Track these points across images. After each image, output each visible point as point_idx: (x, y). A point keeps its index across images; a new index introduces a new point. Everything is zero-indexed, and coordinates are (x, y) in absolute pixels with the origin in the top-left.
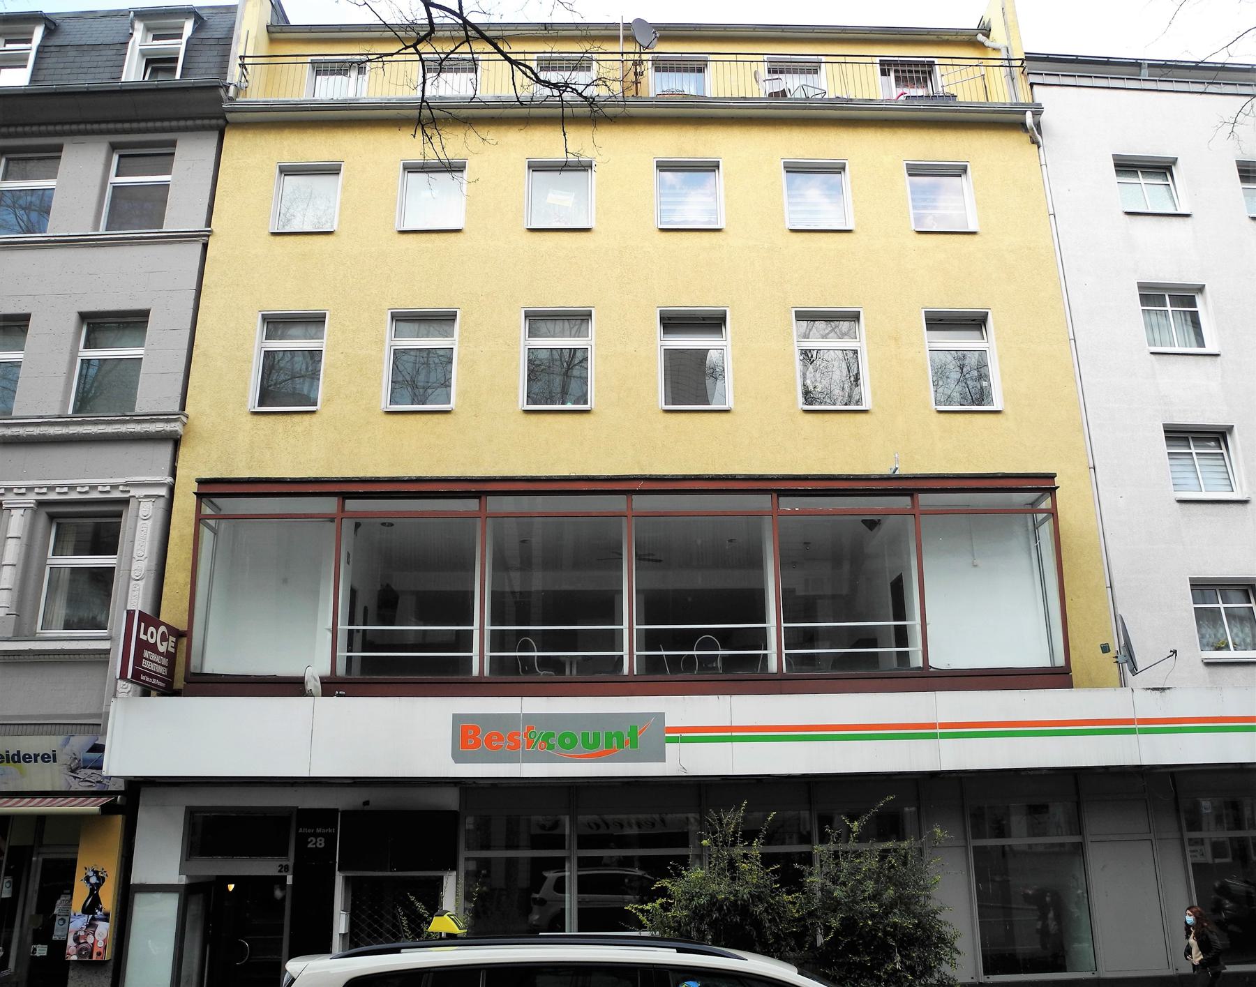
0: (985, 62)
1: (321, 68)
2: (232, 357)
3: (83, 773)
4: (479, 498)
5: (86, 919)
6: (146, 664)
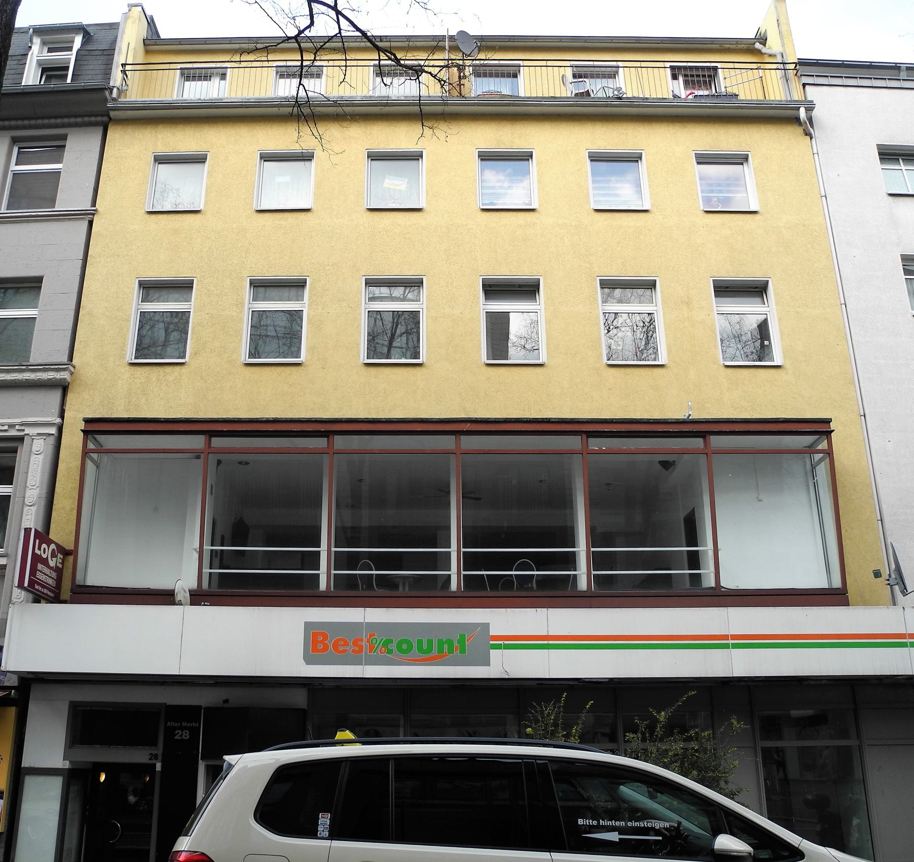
0: (762, 66)
1: (189, 75)
2: (113, 314)
4: (327, 436)
6: (39, 575)
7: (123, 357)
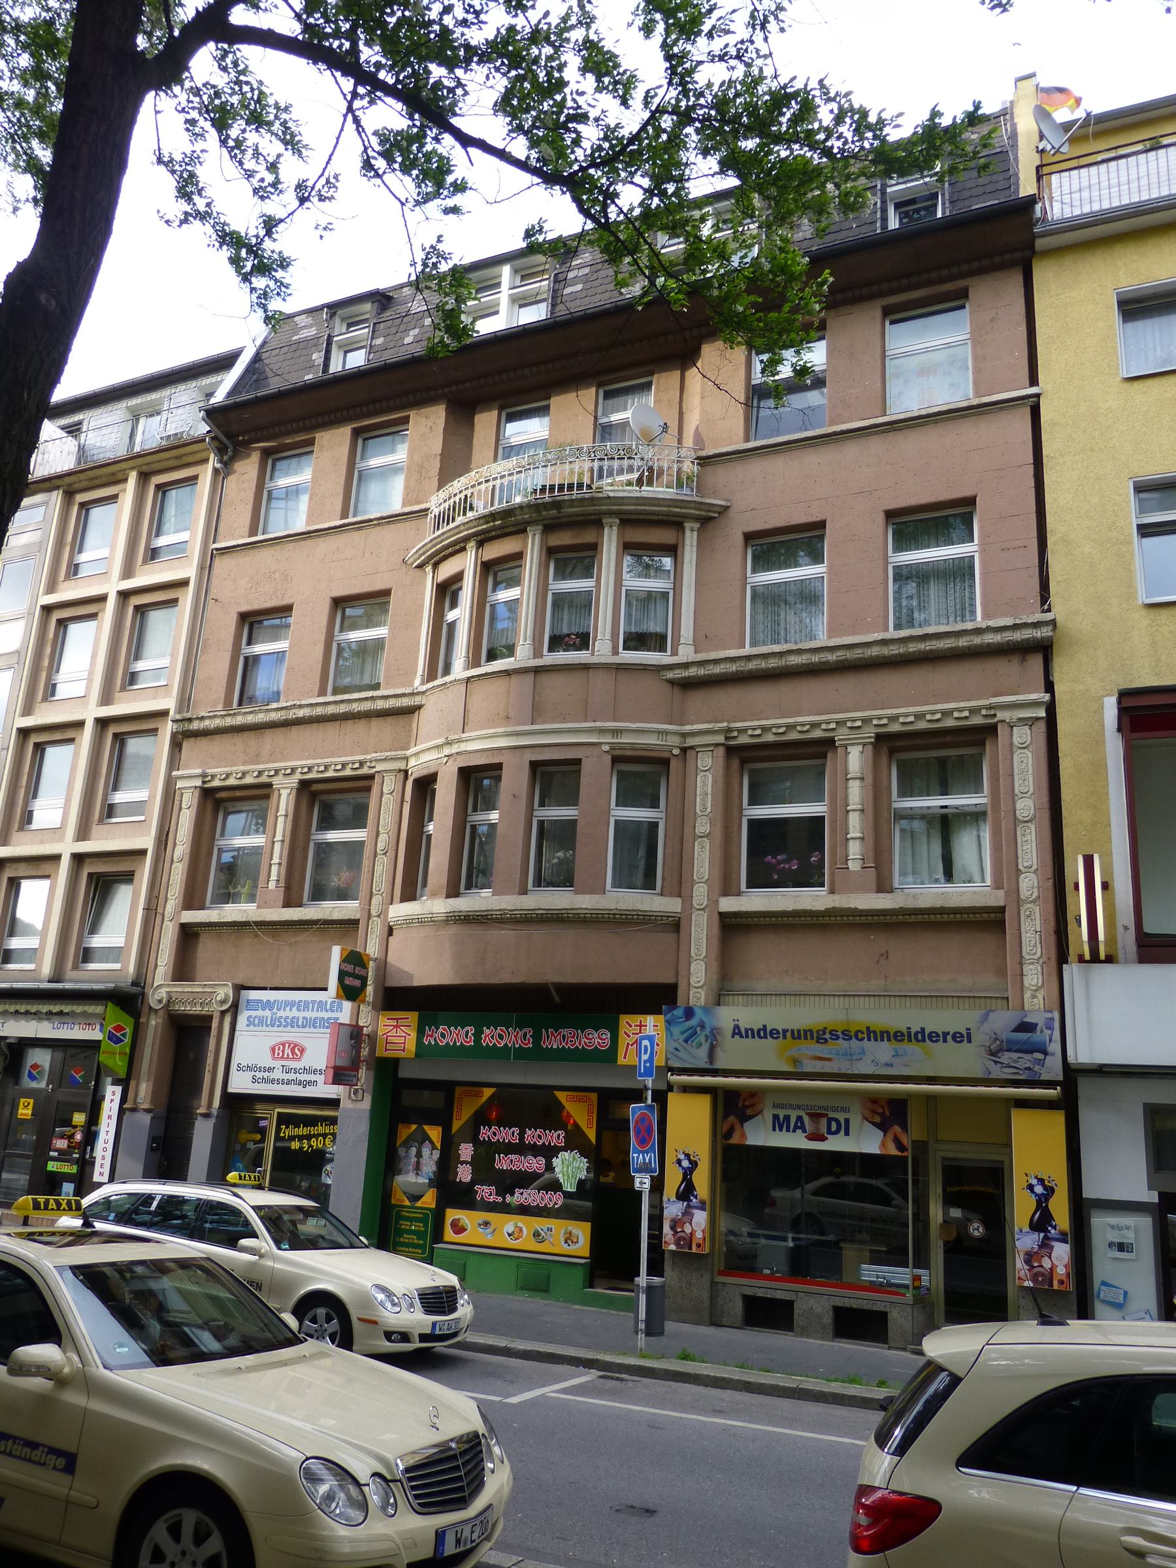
3: (1006, 1057)
7: (1132, 596)
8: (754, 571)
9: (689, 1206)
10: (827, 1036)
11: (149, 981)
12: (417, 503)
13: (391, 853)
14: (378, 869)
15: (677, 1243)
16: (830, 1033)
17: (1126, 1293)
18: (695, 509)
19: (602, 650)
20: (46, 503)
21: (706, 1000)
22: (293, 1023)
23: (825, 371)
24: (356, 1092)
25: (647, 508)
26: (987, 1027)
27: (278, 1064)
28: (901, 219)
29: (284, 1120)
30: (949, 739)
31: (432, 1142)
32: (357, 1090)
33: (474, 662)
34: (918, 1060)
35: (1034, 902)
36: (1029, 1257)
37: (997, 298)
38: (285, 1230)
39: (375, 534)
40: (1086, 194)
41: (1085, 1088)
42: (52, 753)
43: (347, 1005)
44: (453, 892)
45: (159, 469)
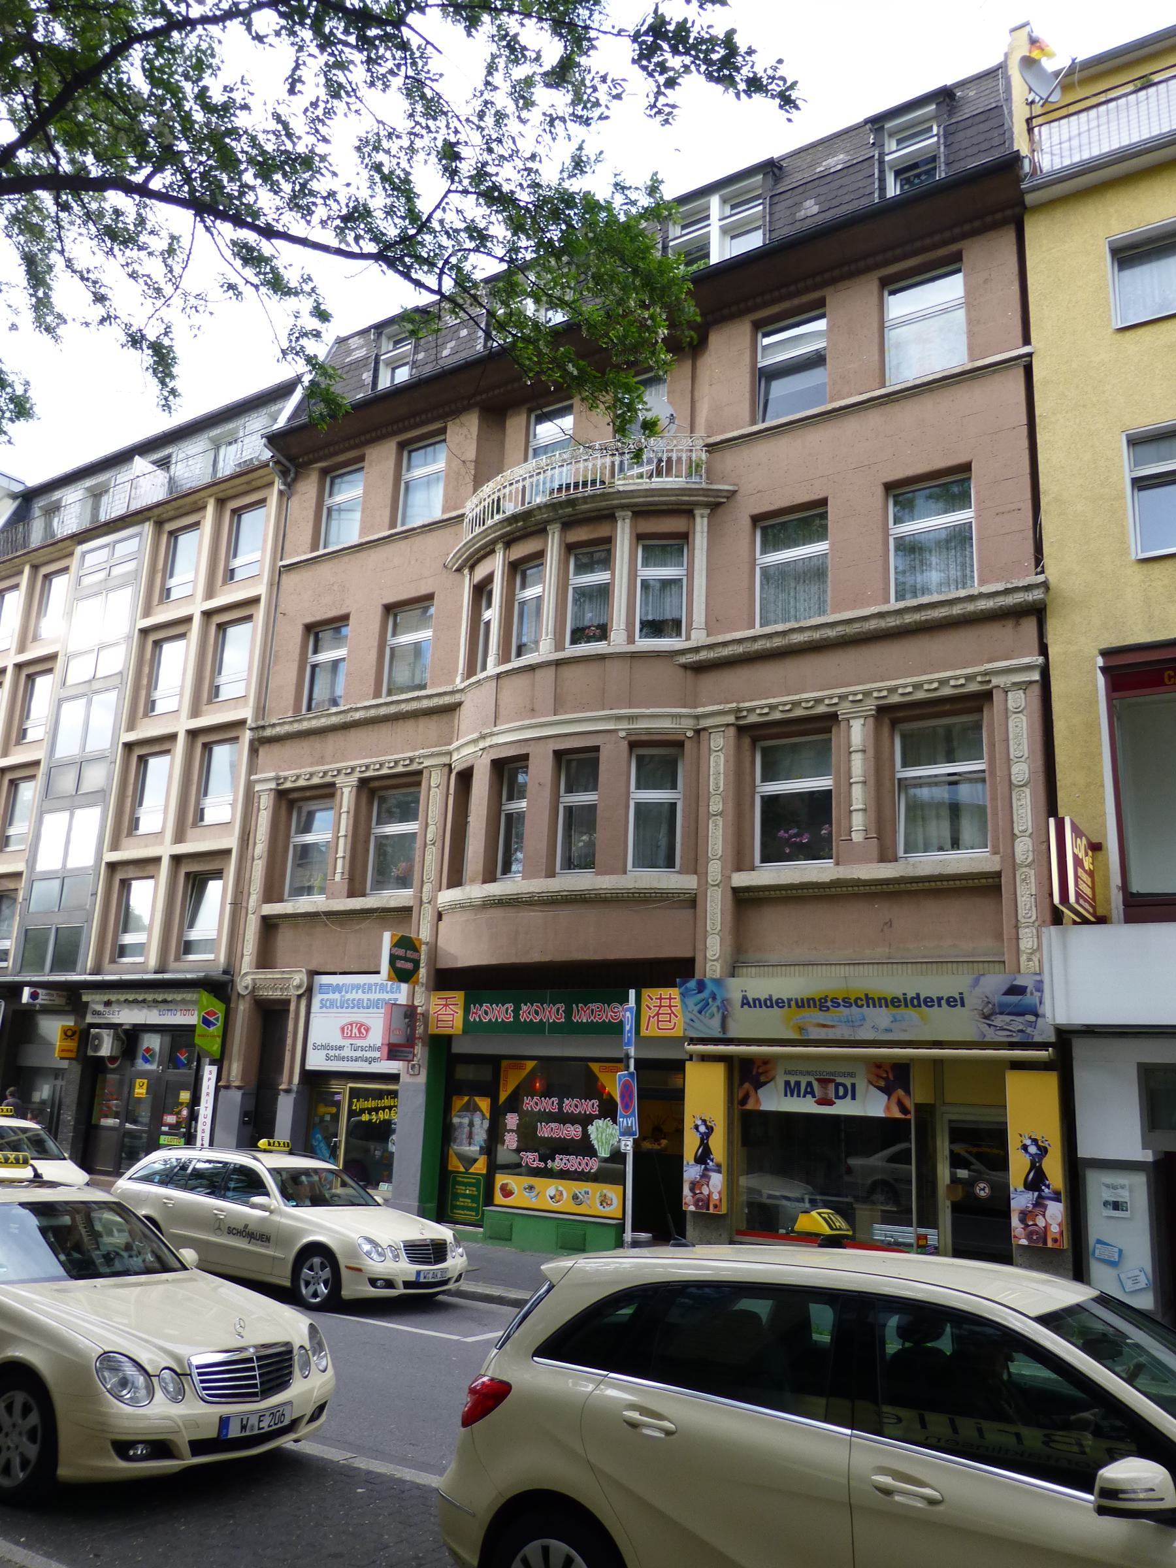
3: (1000, 1020)
5: (699, 1169)
7: (1125, 552)
8: (764, 552)
9: (706, 1169)
10: (829, 1004)
11: (237, 970)
12: (455, 509)
13: (439, 844)
14: (428, 858)
15: (696, 1205)
16: (832, 1001)
17: (1121, 1251)
18: (704, 496)
19: (617, 640)
20: (140, 534)
21: (722, 972)
22: (358, 1004)
23: (825, 348)
24: (413, 1066)
25: (656, 499)
26: (978, 991)
27: (347, 1042)
28: (902, 186)
29: (355, 1094)
30: (947, 707)
31: (481, 1111)
32: (413, 1066)
33: (504, 658)
34: (916, 1025)
35: (1029, 866)
36: (1024, 1216)
37: (992, 256)
38: (295, 1188)
39: (418, 542)
40: (1075, 143)
41: (1080, 1050)
42: (153, 762)
43: (404, 987)
44: (490, 877)
45: (233, 495)
